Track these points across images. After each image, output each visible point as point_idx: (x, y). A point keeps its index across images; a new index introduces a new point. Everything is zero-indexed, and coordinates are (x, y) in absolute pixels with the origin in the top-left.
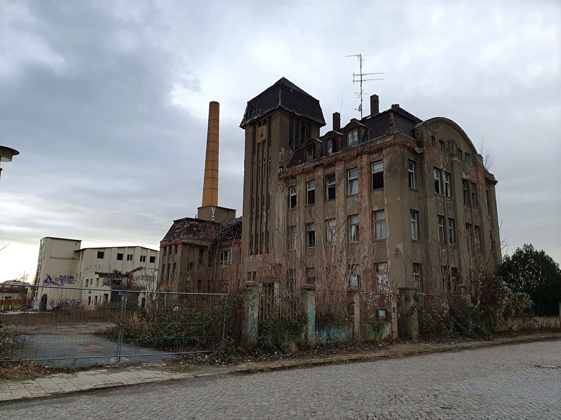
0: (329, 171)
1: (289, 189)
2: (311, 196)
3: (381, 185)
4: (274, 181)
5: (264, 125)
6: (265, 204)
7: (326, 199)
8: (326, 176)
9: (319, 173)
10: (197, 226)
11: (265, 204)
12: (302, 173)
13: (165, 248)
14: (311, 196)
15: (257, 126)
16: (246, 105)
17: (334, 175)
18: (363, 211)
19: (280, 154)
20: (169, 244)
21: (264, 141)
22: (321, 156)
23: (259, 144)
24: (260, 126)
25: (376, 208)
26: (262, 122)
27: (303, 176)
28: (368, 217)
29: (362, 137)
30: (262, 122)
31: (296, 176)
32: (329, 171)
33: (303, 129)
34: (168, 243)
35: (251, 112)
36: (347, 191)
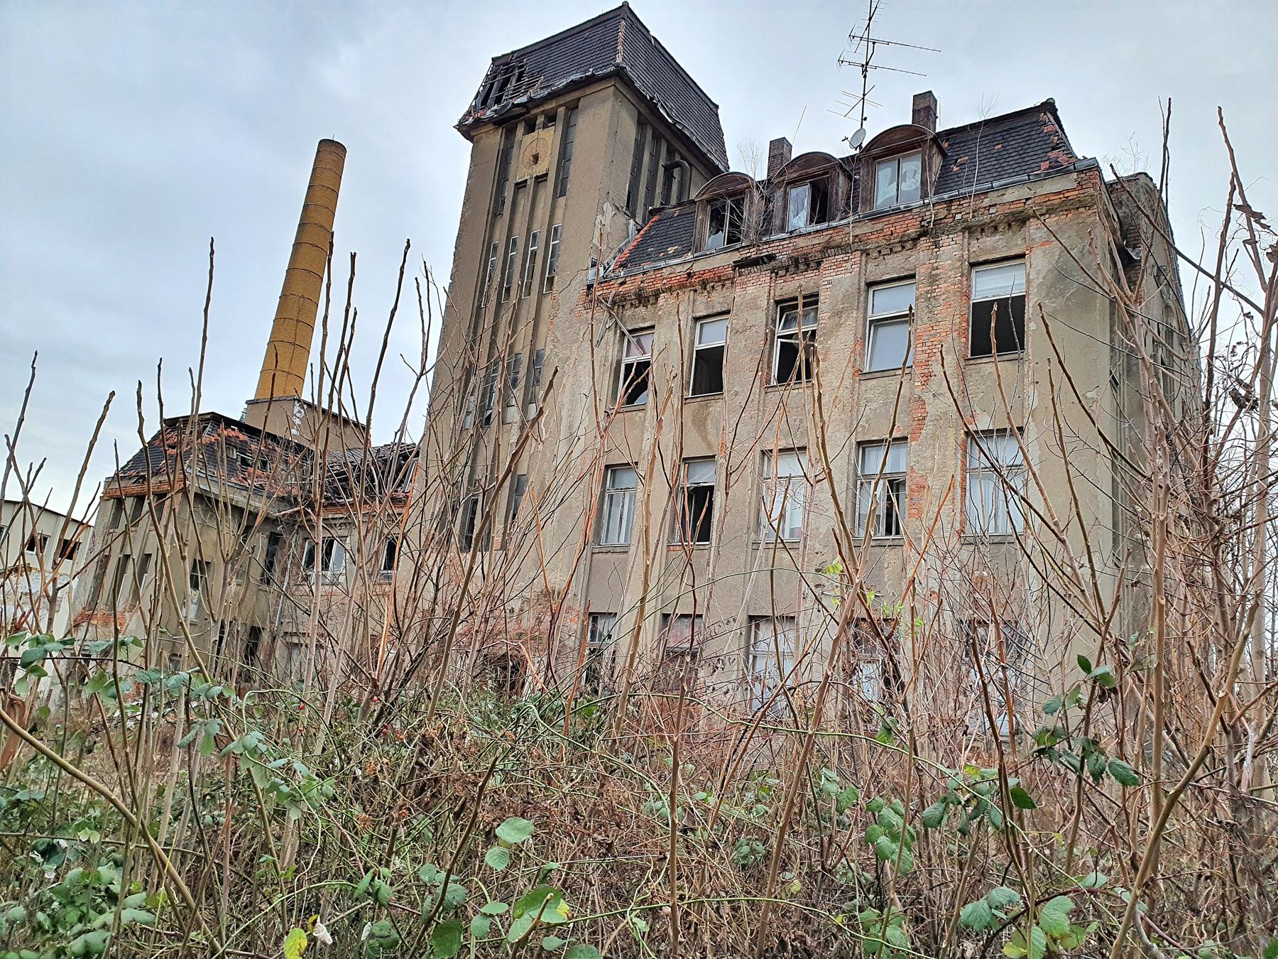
0: (792, 285)
1: (623, 334)
2: (708, 371)
3: (253, 628)
4: (564, 309)
5: (545, 126)
6: (522, 384)
7: (768, 381)
8: (777, 303)
9: (750, 290)
10: (243, 448)
11: (522, 384)
12: (682, 286)
13: (120, 502)
14: (708, 371)
15: (520, 130)
16: (485, 67)
17: (812, 300)
18: (928, 428)
19: (593, 226)
20: (136, 489)
21: (541, 179)
22: (767, 232)
23: (521, 186)
24: (531, 128)
25: (984, 423)
26: (541, 120)
27: (687, 295)
28: (950, 452)
29: (933, 177)
30: (541, 120)
31: (657, 295)
32: (792, 285)
33: (668, 170)
34: (131, 486)
35: (502, 89)
36: (862, 355)
